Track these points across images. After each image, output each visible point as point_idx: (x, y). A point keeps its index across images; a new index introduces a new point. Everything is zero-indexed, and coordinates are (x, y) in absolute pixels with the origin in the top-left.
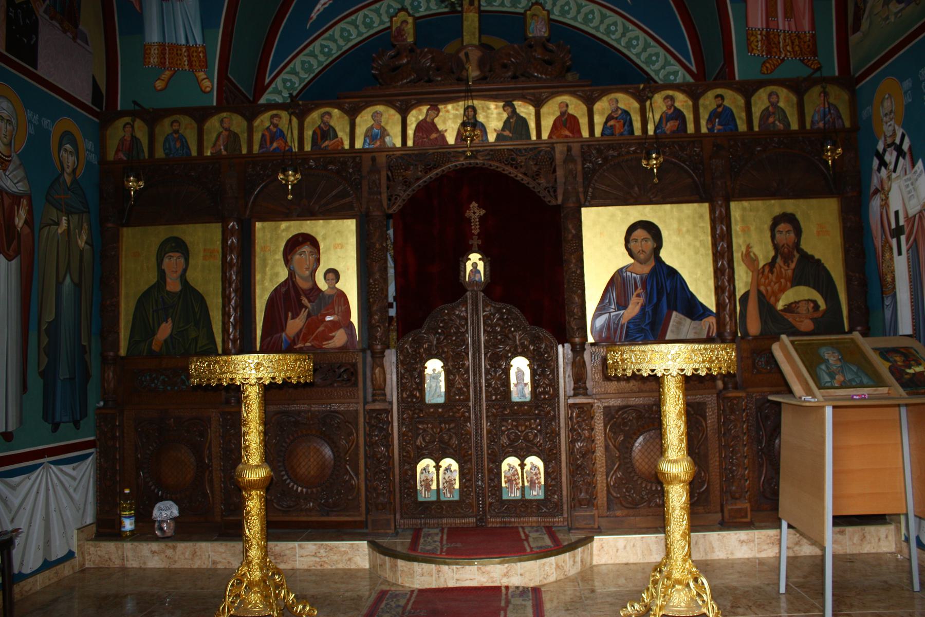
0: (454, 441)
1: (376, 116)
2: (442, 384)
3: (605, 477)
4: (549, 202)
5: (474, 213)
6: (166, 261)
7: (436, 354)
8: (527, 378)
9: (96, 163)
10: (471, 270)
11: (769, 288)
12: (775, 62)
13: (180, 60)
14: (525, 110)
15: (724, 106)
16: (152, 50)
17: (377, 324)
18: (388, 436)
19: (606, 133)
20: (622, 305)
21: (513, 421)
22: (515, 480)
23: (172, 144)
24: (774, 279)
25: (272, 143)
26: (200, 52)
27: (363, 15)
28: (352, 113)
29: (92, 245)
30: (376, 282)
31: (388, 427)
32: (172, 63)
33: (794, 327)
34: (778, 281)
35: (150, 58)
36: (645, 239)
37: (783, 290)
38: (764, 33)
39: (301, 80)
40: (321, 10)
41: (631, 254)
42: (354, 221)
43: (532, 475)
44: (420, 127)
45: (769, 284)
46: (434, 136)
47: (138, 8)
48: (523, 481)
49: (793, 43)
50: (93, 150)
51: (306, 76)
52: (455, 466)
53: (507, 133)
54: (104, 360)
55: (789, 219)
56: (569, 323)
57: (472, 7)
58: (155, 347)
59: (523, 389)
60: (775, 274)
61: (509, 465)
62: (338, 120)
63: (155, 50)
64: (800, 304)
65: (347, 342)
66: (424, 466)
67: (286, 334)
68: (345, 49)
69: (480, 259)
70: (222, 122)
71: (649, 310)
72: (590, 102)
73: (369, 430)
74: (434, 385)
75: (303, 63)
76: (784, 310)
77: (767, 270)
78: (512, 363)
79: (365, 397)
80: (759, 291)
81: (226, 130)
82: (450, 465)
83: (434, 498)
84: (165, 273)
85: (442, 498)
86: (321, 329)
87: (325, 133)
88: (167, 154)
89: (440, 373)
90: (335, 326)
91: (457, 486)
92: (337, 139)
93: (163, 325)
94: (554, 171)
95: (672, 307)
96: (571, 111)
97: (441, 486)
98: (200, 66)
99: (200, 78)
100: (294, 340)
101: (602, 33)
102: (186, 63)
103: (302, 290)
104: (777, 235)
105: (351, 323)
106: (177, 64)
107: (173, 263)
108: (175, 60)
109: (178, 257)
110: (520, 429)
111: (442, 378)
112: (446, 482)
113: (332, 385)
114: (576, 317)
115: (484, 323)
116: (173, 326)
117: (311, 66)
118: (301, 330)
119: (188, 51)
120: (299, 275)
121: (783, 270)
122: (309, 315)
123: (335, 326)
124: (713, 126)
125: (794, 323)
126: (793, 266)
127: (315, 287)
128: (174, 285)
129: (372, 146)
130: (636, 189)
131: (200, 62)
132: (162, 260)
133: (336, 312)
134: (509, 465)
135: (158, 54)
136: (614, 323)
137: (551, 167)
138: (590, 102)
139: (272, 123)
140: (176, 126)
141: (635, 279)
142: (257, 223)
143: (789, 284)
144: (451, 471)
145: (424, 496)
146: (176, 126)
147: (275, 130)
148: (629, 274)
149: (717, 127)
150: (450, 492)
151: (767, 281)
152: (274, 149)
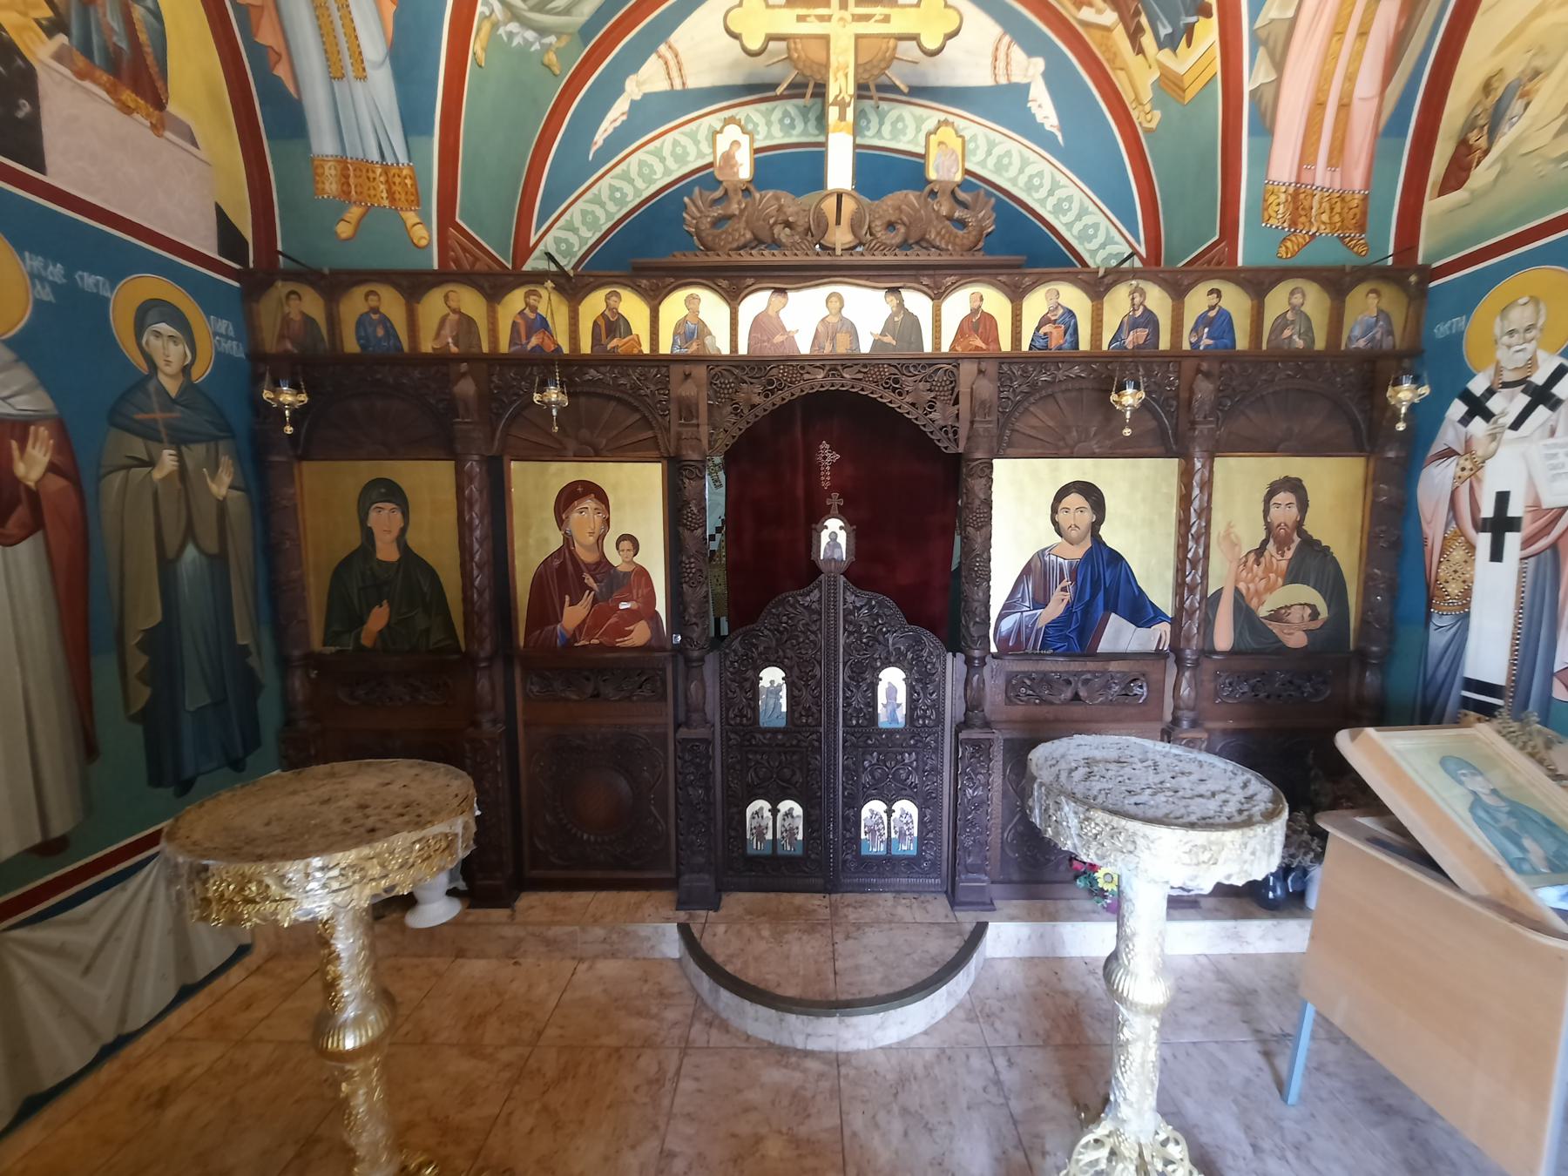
0: (798, 778)
1: (691, 302)
2: (783, 701)
3: (1000, 831)
4: (946, 448)
5: (825, 458)
6: (373, 515)
7: (775, 661)
8: (902, 697)
9: (243, 356)
10: (828, 543)
11: (1251, 586)
12: (1301, 240)
13: (374, 189)
14: (917, 302)
15: (1220, 307)
16: (326, 168)
17: (694, 620)
18: (707, 776)
19: (1037, 344)
20: (1041, 602)
21: (879, 754)
22: (879, 830)
23: (370, 330)
24: (1260, 574)
25: (528, 338)
26: (405, 178)
27: (672, 140)
28: (654, 298)
29: (246, 490)
30: (692, 560)
31: (708, 763)
32: (361, 193)
33: (1280, 641)
34: (1266, 576)
35: (323, 183)
36: (1081, 509)
37: (1270, 589)
38: (1291, 190)
39: (583, 241)
40: (610, 130)
41: (1059, 532)
42: (660, 465)
43: (901, 825)
44: (757, 323)
45: (1252, 581)
46: (778, 339)
47: (292, 90)
48: (889, 832)
49: (1332, 209)
50: (232, 334)
51: (590, 235)
52: (798, 810)
53: (888, 339)
54: (284, 664)
55: (1294, 486)
56: (968, 628)
57: (843, 123)
58: (366, 641)
59: (895, 711)
60: (1263, 565)
61: (872, 811)
62: (632, 307)
63: (330, 168)
64: (1292, 609)
65: (651, 639)
66: (757, 809)
67: (562, 626)
68: (646, 194)
69: (841, 528)
70: (446, 297)
71: (1078, 609)
72: (1017, 295)
73: (682, 767)
74: (771, 702)
75: (584, 213)
76: (1268, 618)
77: (1252, 557)
78: (881, 676)
79: (676, 717)
80: (1237, 590)
81: (455, 311)
82: (791, 809)
83: (769, 851)
84: (372, 533)
85: (780, 852)
86: (613, 620)
87: (613, 325)
88: (362, 347)
89: (780, 686)
90: (633, 616)
91: (800, 837)
92: (630, 337)
93: (376, 610)
94: (956, 402)
95: (1112, 607)
96: (987, 307)
97: (779, 836)
98: (407, 201)
99: (409, 224)
100: (574, 635)
101: (1021, 188)
102: (385, 195)
103: (585, 564)
104: (1273, 510)
105: (657, 613)
106: (369, 196)
107: (384, 519)
108: (366, 188)
109: (392, 511)
110: (888, 764)
111: (784, 693)
112: (786, 831)
113: (629, 698)
114: (978, 620)
115: (844, 619)
116: (391, 611)
117: (596, 219)
118: (584, 621)
119: (386, 174)
120: (581, 545)
121: (1274, 560)
122: (595, 601)
123: (633, 616)
124: (1200, 339)
125: (1280, 635)
126: (1289, 554)
127: (603, 562)
128: (387, 551)
129: (684, 351)
130: (1075, 434)
131: (407, 193)
132: (367, 514)
133: (635, 597)
134: (872, 811)
135: (336, 175)
136: (1027, 627)
138: (1017, 295)
139: (527, 304)
140: (373, 301)
141: (1061, 564)
142: (513, 463)
143: (1280, 581)
144: (792, 817)
145: (755, 846)
146: (373, 301)
147: (532, 316)
148: (1053, 558)
150: (791, 844)
151: (1250, 575)
152: (533, 348)
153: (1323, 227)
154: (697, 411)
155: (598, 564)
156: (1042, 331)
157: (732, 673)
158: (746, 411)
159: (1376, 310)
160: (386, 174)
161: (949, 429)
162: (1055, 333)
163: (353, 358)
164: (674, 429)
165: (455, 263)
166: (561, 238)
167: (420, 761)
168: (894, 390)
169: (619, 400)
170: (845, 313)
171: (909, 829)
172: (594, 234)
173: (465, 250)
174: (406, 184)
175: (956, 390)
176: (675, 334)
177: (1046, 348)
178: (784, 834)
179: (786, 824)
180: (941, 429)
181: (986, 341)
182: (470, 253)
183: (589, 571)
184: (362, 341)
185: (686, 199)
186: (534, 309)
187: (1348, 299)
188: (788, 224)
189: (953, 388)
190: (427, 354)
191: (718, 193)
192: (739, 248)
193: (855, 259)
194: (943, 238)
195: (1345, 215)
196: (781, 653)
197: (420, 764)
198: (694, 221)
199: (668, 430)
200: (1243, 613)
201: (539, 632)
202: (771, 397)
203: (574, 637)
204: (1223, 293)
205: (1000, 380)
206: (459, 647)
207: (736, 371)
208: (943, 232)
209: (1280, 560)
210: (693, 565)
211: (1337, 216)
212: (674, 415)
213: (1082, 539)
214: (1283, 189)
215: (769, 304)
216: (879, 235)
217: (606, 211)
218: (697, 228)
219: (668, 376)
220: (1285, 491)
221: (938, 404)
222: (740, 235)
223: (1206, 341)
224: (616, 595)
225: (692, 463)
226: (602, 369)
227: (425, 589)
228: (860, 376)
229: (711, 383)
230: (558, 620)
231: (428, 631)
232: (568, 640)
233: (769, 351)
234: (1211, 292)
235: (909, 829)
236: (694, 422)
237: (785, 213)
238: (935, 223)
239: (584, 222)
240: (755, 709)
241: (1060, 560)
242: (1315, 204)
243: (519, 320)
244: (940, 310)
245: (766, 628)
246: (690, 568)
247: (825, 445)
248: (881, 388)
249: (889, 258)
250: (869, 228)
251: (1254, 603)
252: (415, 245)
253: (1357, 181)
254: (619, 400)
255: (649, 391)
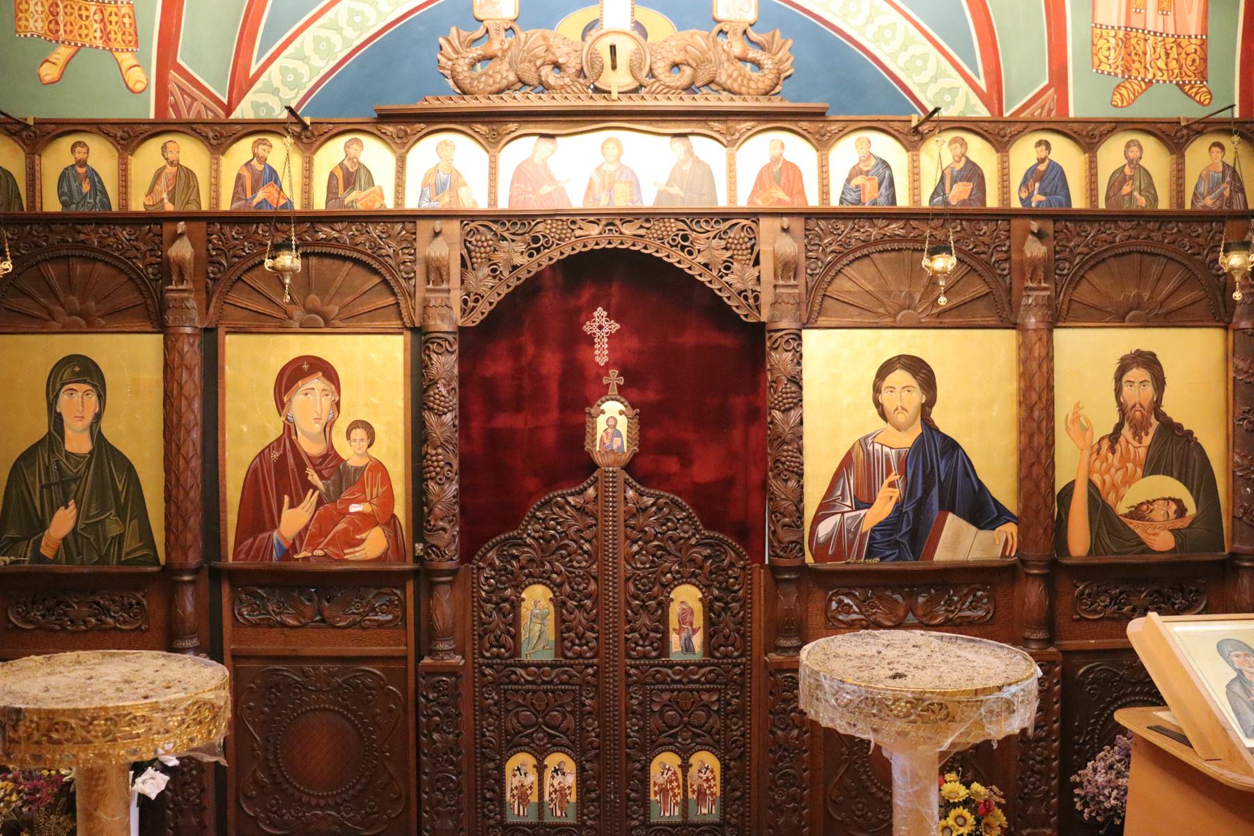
5: (601, 327)
6: (64, 398)
11: (1107, 478)
12: (1136, 87)
13: (87, 28)
15: (1051, 161)
19: (848, 197)
20: (863, 502)
22: (672, 789)
23: (74, 185)
25: (254, 191)
26: (124, 16)
32: (71, 32)
33: (1144, 543)
35: (27, 20)
37: (1128, 482)
38: (1121, 34)
41: (883, 415)
46: (546, 189)
48: (685, 791)
49: (1167, 54)
51: (322, 63)
52: (570, 766)
53: (675, 190)
55: (1148, 361)
60: (1118, 454)
67: (279, 533)
69: (621, 413)
71: (909, 508)
74: (537, 628)
77: (1105, 444)
80: (1091, 483)
83: (533, 818)
84: (62, 420)
86: (342, 526)
87: (350, 177)
88: (64, 204)
90: (367, 521)
94: (757, 262)
95: (948, 506)
96: (789, 156)
97: (547, 798)
98: (124, 41)
99: (124, 67)
102: (98, 34)
104: (1126, 389)
105: (394, 516)
109: (86, 393)
112: (555, 791)
118: (306, 528)
119: (102, 12)
120: (303, 433)
122: (320, 502)
123: (367, 521)
124: (1031, 195)
125: (1143, 536)
126: (1147, 440)
128: (78, 442)
132: (57, 396)
133: (369, 498)
136: (849, 531)
137: (751, 254)
142: (228, 337)
143: (1139, 471)
144: (564, 774)
147: (260, 167)
148: (878, 447)
149: (1037, 198)
152: (259, 203)
153: (1159, 74)
154: (448, 274)
155: (324, 457)
156: (855, 182)
157: (487, 592)
158: (506, 274)
159: (1221, 164)
160: (102, 12)
161: (749, 294)
162: (867, 183)
163: (50, 220)
164: (419, 296)
165: (174, 110)
166: (287, 68)
167: (165, 653)
168: (683, 248)
169: (357, 262)
170: (624, 160)
171: (710, 787)
172: (327, 62)
173: (182, 91)
174: (124, 24)
175: (756, 249)
176: (424, 185)
177: (859, 202)
178: (554, 796)
179: (556, 783)
180: (739, 294)
181: (790, 193)
182: (212, 111)
183: (314, 466)
184: (64, 198)
185: (442, 41)
186: (262, 160)
187: (1188, 154)
188: (557, 66)
189: (754, 245)
190: (137, 213)
191: (480, 32)
192: (500, 92)
193: (636, 103)
194: (735, 80)
195: (1183, 61)
196: (548, 566)
197: (164, 656)
198: (450, 63)
199: (412, 296)
200: (1099, 507)
201: (250, 541)
202: (536, 256)
203: (294, 548)
204: (1052, 145)
205: (806, 236)
206: (158, 559)
207: (494, 227)
208: (735, 75)
209: (1138, 447)
210: (441, 457)
211: (1174, 62)
212: (420, 278)
213: (911, 424)
214: (1113, 33)
215: (535, 152)
216: (661, 77)
217: (343, 38)
218: (452, 71)
219: (415, 233)
220: (1138, 366)
221: (736, 266)
222: (502, 78)
223: (1037, 198)
224: (345, 496)
225: (441, 335)
226: (339, 226)
227: (120, 488)
228: (642, 232)
229: (465, 240)
230: (274, 526)
231: (120, 538)
232: (287, 551)
233: (533, 204)
234: (1039, 143)
235: (710, 787)
236: (444, 286)
237: (554, 54)
238: (726, 65)
239: (316, 50)
240: (516, 637)
241: (887, 450)
242: (1149, 50)
243: (246, 173)
244: (734, 158)
245: (529, 535)
246: (438, 461)
247: (600, 312)
248: (667, 246)
249: (674, 103)
250: (651, 69)
251: (1111, 499)
252: (132, 91)
253: (1192, 25)
254: (357, 262)
255: (391, 251)
